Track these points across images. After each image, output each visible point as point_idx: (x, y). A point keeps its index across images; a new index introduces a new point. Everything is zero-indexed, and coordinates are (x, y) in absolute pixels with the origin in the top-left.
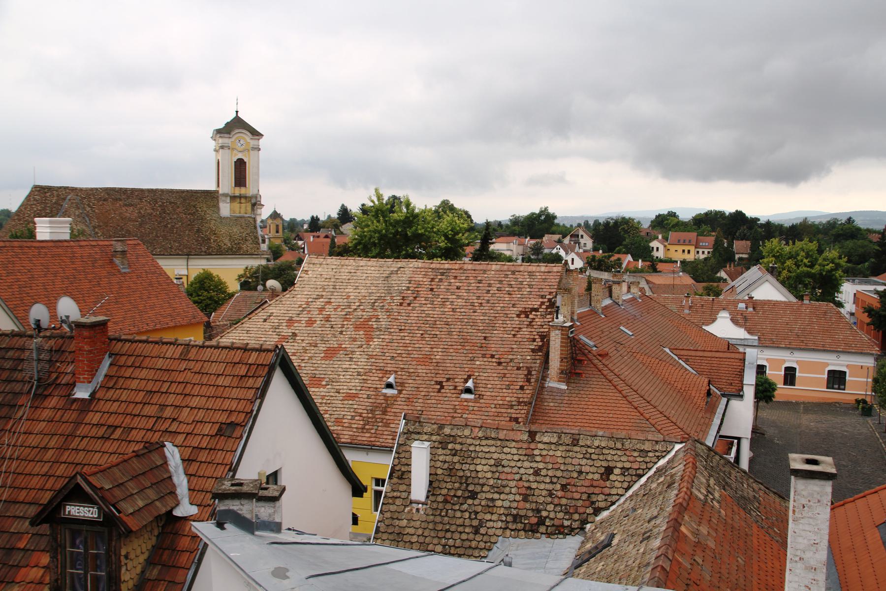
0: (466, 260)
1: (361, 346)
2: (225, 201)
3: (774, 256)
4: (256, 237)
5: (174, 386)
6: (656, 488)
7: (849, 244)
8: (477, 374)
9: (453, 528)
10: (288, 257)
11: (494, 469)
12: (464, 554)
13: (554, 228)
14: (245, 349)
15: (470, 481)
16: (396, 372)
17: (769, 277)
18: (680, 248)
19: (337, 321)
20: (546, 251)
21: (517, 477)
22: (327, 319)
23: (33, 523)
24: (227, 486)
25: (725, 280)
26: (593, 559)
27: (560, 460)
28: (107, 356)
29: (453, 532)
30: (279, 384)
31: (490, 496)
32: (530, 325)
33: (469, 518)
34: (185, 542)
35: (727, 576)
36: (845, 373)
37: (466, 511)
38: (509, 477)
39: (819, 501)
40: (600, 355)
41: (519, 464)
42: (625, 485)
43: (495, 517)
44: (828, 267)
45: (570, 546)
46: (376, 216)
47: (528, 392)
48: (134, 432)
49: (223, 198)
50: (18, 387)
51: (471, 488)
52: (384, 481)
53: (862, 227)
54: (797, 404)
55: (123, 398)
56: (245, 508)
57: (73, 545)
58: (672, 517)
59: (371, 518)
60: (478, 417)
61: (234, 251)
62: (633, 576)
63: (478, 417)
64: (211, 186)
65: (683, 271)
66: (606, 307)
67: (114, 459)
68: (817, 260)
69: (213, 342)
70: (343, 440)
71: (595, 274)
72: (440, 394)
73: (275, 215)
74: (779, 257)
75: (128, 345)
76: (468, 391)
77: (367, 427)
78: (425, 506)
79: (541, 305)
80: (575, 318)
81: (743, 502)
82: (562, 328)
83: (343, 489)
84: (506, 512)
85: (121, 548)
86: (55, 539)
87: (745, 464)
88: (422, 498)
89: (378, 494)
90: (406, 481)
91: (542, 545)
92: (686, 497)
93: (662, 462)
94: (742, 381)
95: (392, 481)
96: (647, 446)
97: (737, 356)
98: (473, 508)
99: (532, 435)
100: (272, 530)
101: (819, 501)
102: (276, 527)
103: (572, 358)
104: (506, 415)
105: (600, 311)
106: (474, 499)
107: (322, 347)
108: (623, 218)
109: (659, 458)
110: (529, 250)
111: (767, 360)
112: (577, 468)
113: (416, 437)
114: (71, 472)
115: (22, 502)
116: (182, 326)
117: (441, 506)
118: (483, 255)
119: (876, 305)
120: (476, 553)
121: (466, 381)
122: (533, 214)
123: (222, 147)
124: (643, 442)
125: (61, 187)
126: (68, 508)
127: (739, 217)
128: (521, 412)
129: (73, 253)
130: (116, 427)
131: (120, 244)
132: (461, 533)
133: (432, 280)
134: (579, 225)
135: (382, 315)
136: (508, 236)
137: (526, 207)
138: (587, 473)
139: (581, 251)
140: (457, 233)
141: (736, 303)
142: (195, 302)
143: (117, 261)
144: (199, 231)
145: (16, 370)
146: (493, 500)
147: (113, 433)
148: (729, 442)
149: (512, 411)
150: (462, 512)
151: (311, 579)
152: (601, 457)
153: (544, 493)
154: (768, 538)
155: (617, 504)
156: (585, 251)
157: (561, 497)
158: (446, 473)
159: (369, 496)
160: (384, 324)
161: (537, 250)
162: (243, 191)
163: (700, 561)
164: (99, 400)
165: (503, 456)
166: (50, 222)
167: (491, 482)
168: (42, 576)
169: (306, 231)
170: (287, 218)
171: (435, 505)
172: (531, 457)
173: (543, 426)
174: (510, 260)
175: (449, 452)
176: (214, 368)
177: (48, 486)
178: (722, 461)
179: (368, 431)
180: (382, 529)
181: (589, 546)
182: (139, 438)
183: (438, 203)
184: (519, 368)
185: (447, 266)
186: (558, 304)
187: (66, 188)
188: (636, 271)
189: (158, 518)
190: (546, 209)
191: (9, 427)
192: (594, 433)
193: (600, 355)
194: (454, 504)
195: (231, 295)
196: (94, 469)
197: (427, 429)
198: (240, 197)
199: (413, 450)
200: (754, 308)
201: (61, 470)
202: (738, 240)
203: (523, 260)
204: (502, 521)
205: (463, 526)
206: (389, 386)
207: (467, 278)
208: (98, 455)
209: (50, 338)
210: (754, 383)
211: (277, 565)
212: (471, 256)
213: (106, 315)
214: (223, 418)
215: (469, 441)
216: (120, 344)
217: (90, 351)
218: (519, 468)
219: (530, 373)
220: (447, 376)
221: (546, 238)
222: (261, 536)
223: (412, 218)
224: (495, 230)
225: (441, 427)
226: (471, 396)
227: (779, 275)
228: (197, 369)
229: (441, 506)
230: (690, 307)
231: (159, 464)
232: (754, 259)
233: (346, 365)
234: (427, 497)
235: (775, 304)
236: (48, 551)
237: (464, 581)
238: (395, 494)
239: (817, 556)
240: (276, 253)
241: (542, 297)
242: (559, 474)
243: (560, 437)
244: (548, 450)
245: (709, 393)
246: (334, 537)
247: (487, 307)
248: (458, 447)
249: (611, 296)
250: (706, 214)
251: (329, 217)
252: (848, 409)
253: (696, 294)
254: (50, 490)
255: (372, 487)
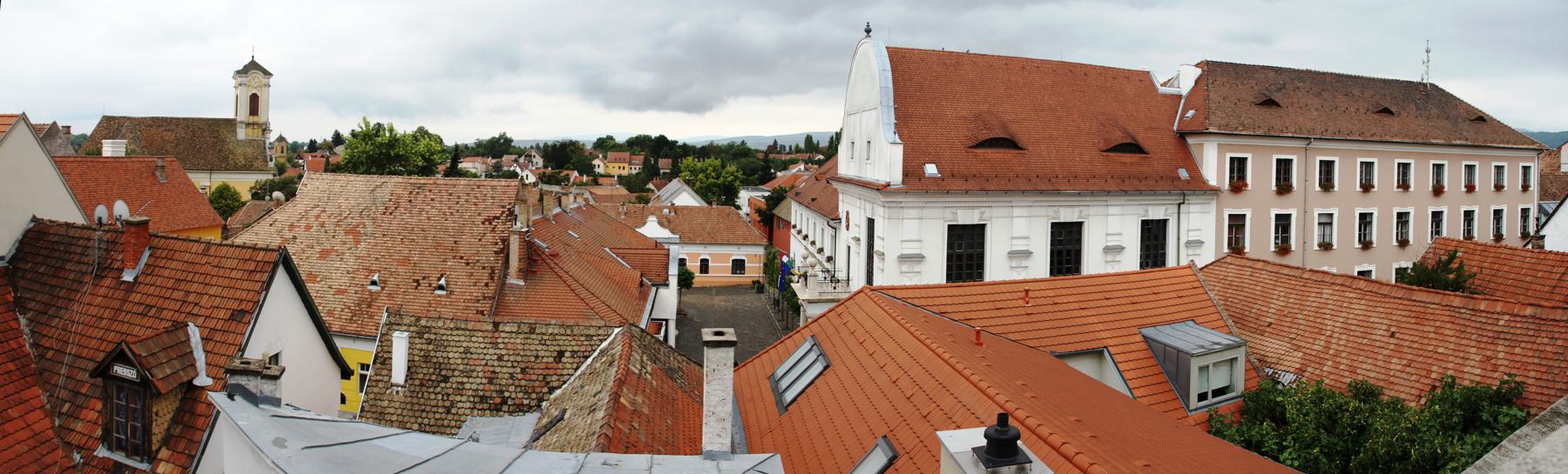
0: (439, 176)
1: (350, 249)
2: (241, 128)
3: (689, 171)
4: (266, 157)
5: (197, 276)
6: (600, 367)
7: (744, 160)
8: (448, 273)
9: (428, 409)
10: (290, 173)
11: (464, 356)
12: (437, 432)
13: (511, 150)
14: (254, 248)
15: (443, 366)
16: (379, 271)
17: (686, 187)
18: (617, 165)
19: (330, 227)
20: (505, 169)
21: (483, 362)
22: (322, 225)
23: (91, 376)
24: (237, 363)
25: (653, 191)
26: (548, 433)
27: (520, 347)
28: (147, 249)
29: (428, 412)
30: (281, 280)
31: (460, 380)
32: (493, 230)
33: (442, 399)
34: (201, 408)
35: (658, 435)
36: (744, 261)
37: (439, 393)
38: (477, 362)
39: (725, 365)
40: (552, 255)
41: (485, 351)
42: (575, 366)
43: (464, 399)
44: (729, 179)
45: (529, 422)
46: (364, 140)
47: (492, 288)
48: (165, 312)
49: (240, 125)
50: (84, 268)
51: (444, 373)
52: (368, 366)
53: (752, 148)
54: (711, 288)
55: (158, 283)
56: (253, 384)
57: (118, 398)
58: (613, 390)
59: (357, 399)
60: (450, 310)
61: (247, 167)
62: (582, 445)
63: (450, 310)
64: (232, 116)
65: (620, 184)
66: (557, 215)
67: (149, 332)
68: (721, 173)
69: (229, 242)
70: (334, 329)
71: (546, 187)
72: (417, 291)
73: (281, 139)
74: (694, 172)
75: (163, 240)
76: (441, 288)
77: (355, 318)
78: (404, 389)
79: (502, 214)
80: (531, 224)
81: (670, 373)
82: (520, 233)
83: (336, 372)
84: (474, 394)
85: (152, 406)
86: (106, 391)
87: (672, 342)
88: (402, 382)
89: (363, 377)
90: (388, 367)
91: (505, 422)
92: (624, 373)
93: (604, 344)
94: (667, 272)
95: (376, 366)
96: (592, 331)
97: (663, 252)
98: (445, 391)
99: (496, 325)
100: (273, 405)
101: (725, 365)
102: (276, 402)
103: (528, 258)
104: (473, 308)
105: (551, 218)
106: (446, 382)
107: (318, 249)
108: (571, 141)
109: (601, 341)
110: (491, 168)
111: (687, 254)
112: (535, 353)
113: (397, 327)
114: (117, 339)
115: (84, 358)
116: (204, 228)
117: (417, 389)
118: (453, 172)
119: (764, 207)
120: (448, 431)
121: (439, 279)
122: (494, 138)
123: (240, 85)
124: (589, 327)
125: (120, 117)
126: (116, 368)
127: (662, 140)
128: (485, 306)
129: (127, 166)
130: (152, 307)
131: (160, 160)
132: (435, 413)
133: (411, 193)
134: (532, 147)
135: (368, 223)
136: (474, 156)
137: (488, 133)
138: (543, 357)
139: (534, 168)
140: (432, 154)
141: (661, 209)
142: (215, 208)
143: (158, 174)
144: (220, 151)
145: (84, 254)
146: (462, 383)
147: (150, 310)
148: (659, 323)
149: (479, 305)
150: (436, 394)
151: (305, 450)
152: (554, 343)
153: (507, 376)
154: (690, 400)
155: (568, 383)
156: (537, 169)
157: (521, 379)
158: (422, 359)
159: (355, 379)
160: (370, 229)
161: (498, 168)
162: (255, 119)
163: (636, 425)
164: (140, 283)
165: (471, 345)
166: (113, 143)
167: (461, 367)
168: (97, 418)
169: (306, 152)
170: (290, 141)
171: (412, 388)
172: (495, 345)
173: (505, 317)
174: (475, 176)
175: (424, 341)
176: (229, 263)
177: (102, 348)
178: (653, 340)
179: (355, 322)
180: (366, 409)
181: (545, 421)
182: (168, 317)
183: (415, 129)
184: (484, 268)
185: (423, 181)
186: (516, 213)
187: (124, 117)
188: (582, 184)
189: (181, 385)
190: (504, 134)
191: (77, 298)
192: (548, 322)
193: (552, 255)
194: (428, 387)
195: (244, 204)
196: (135, 339)
197: (406, 320)
198: (253, 124)
199: (394, 339)
200: (675, 213)
201: (111, 336)
202: (662, 158)
203: (486, 176)
204: (470, 402)
205: (437, 406)
206: (374, 283)
207: (440, 191)
208: (138, 328)
209: (108, 231)
210: (677, 273)
211: (278, 436)
212: (443, 172)
213: (148, 216)
214: (235, 305)
215: (442, 331)
216: (157, 240)
217: (135, 244)
218: (485, 354)
219: (493, 272)
220: (423, 275)
221: (505, 158)
222: (264, 409)
223: (394, 141)
224: (462, 151)
225: (418, 319)
226: (444, 293)
227: (694, 186)
228: (215, 263)
229: (417, 389)
230: (626, 214)
231: (183, 340)
232: (675, 173)
233: (338, 264)
234: (406, 381)
235: (695, 207)
236: (101, 400)
237: (438, 456)
238: (378, 378)
239: (725, 409)
240: (281, 169)
241: (503, 207)
242: (519, 359)
243: (519, 327)
244: (510, 338)
245: (642, 284)
246: (325, 414)
247: (456, 215)
248: (433, 337)
249: (560, 205)
250: (637, 138)
251: (325, 140)
252: (747, 289)
253: (630, 202)
254: (103, 351)
255: (358, 371)
